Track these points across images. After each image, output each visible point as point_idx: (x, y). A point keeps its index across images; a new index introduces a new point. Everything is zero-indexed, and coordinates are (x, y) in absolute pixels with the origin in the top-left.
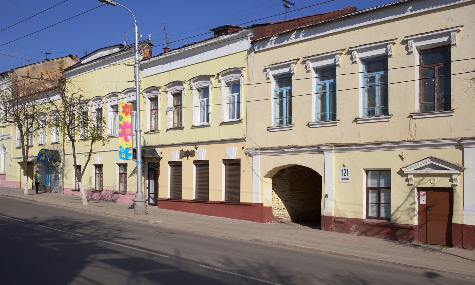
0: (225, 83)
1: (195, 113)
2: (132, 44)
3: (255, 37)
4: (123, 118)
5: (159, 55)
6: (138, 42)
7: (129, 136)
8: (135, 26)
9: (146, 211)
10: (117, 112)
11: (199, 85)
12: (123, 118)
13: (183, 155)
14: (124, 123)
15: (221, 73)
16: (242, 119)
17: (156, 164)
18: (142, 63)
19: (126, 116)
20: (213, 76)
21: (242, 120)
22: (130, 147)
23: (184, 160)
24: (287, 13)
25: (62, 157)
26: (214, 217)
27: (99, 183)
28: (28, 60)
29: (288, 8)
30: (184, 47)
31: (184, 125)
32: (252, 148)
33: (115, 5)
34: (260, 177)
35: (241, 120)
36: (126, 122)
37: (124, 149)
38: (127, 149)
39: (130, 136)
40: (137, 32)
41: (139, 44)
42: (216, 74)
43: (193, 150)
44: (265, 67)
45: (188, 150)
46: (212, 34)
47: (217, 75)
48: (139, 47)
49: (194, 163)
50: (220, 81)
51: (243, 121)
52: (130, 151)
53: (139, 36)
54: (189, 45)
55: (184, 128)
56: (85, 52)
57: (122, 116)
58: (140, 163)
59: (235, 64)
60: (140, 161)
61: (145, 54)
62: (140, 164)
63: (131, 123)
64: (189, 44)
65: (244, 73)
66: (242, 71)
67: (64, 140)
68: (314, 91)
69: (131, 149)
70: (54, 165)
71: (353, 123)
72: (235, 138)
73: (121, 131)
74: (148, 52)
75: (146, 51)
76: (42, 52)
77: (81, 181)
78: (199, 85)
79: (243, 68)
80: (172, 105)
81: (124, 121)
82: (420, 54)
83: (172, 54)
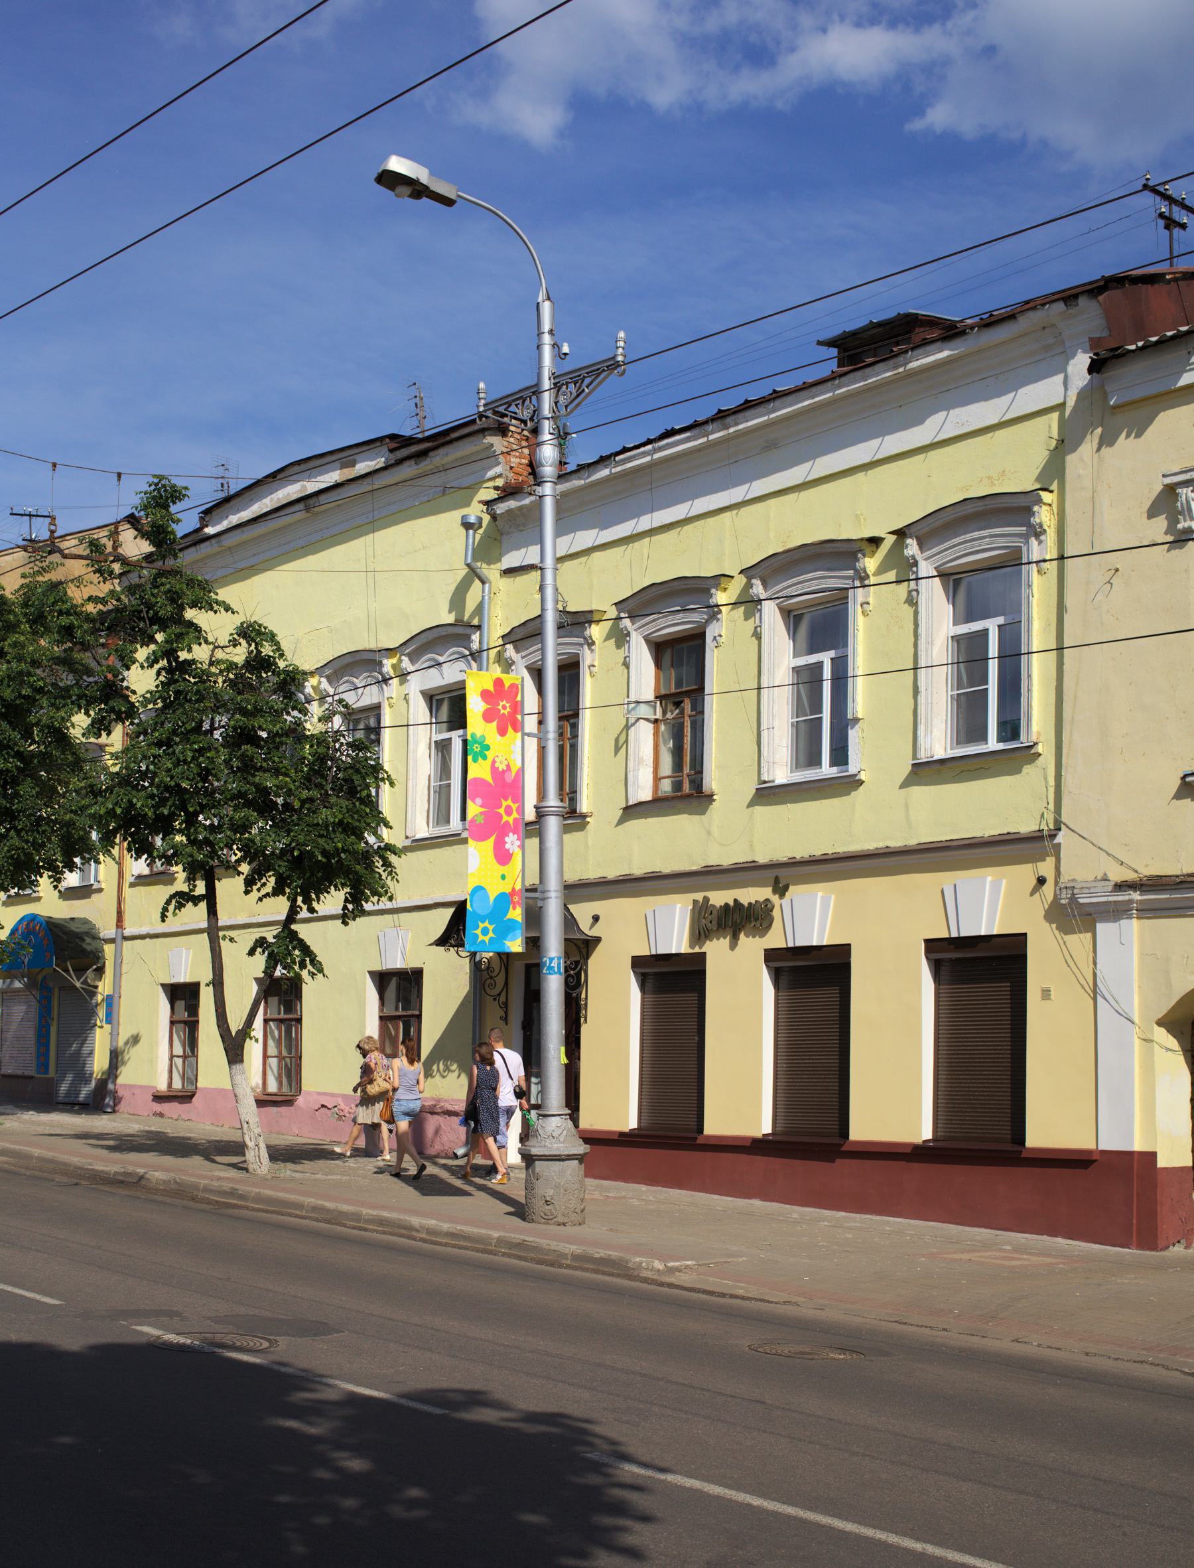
0: (779, 608)
1: (776, 724)
2: (520, 391)
3: (1110, 335)
4: (488, 748)
5: (590, 465)
6: (554, 376)
7: (511, 834)
8: (540, 300)
9: (582, 1207)
10: (458, 719)
11: (949, 555)
12: (488, 748)
13: (714, 926)
14: (494, 769)
15: (918, 526)
16: (1034, 738)
17: (573, 969)
18: (501, 508)
19: (499, 738)
20: (875, 541)
21: (1035, 744)
22: (514, 889)
23: (716, 950)
24: (1168, 257)
25: (109, 950)
26: (891, 1219)
27: (280, 1062)
28: (54, 465)
29: (1176, 231)
30: (721, 416)
31: (713, 779)
32: (1096, 880)
33: (448, 202)
34: (1136, 1020)
35: (1031, 747)
36: (501, 767)
37: (492, 901)
38: (505, 900)
39: (516, 836)
40: (551, 332)
41: (557, 387)
42: (890, 533)
43: (767, 900)
44: (1168, 481)
45: (736, 900)
46: (829, 360)
47: (894, 537)
48: (556, 403)
49: (766, 961)
50: (511, 665)
51: (1040, 748)
52: (514, 908)
53: (556, 346)
54: (747, 406)
55: (715, 797)
56: (222, 485)
57: (483, 737)
58: (559, 968)
59: (989, 478)
60: (559, 958)
61: (511, 468)
62: (560, 974)
63: (517, 773)
64: (747, 401)
65: (1045, 516)
66: (1036, 508)
67: (121, 874)
68: (860, 681)
69: (516, 899)
70: (78, 984)
71: (621, 826)
72: (996, 833)
73: (481, 813)
74: (525, 461)
75: (517, 457)
76: (14, 512)
77: (242, 1061)
78: (949, 555)
79: (1041, 493)
80: (649, 694)
81: (494, 762)
82: (658, 664)
83: (656, 456)
